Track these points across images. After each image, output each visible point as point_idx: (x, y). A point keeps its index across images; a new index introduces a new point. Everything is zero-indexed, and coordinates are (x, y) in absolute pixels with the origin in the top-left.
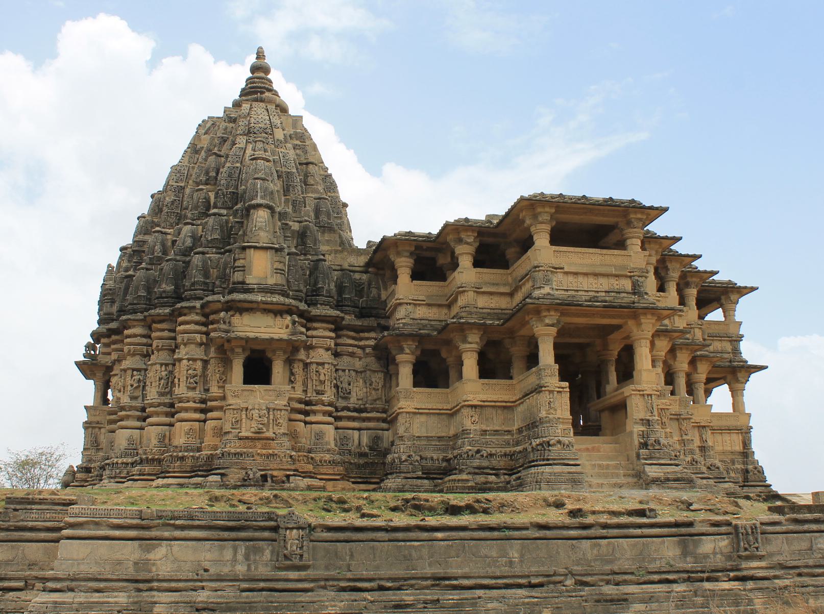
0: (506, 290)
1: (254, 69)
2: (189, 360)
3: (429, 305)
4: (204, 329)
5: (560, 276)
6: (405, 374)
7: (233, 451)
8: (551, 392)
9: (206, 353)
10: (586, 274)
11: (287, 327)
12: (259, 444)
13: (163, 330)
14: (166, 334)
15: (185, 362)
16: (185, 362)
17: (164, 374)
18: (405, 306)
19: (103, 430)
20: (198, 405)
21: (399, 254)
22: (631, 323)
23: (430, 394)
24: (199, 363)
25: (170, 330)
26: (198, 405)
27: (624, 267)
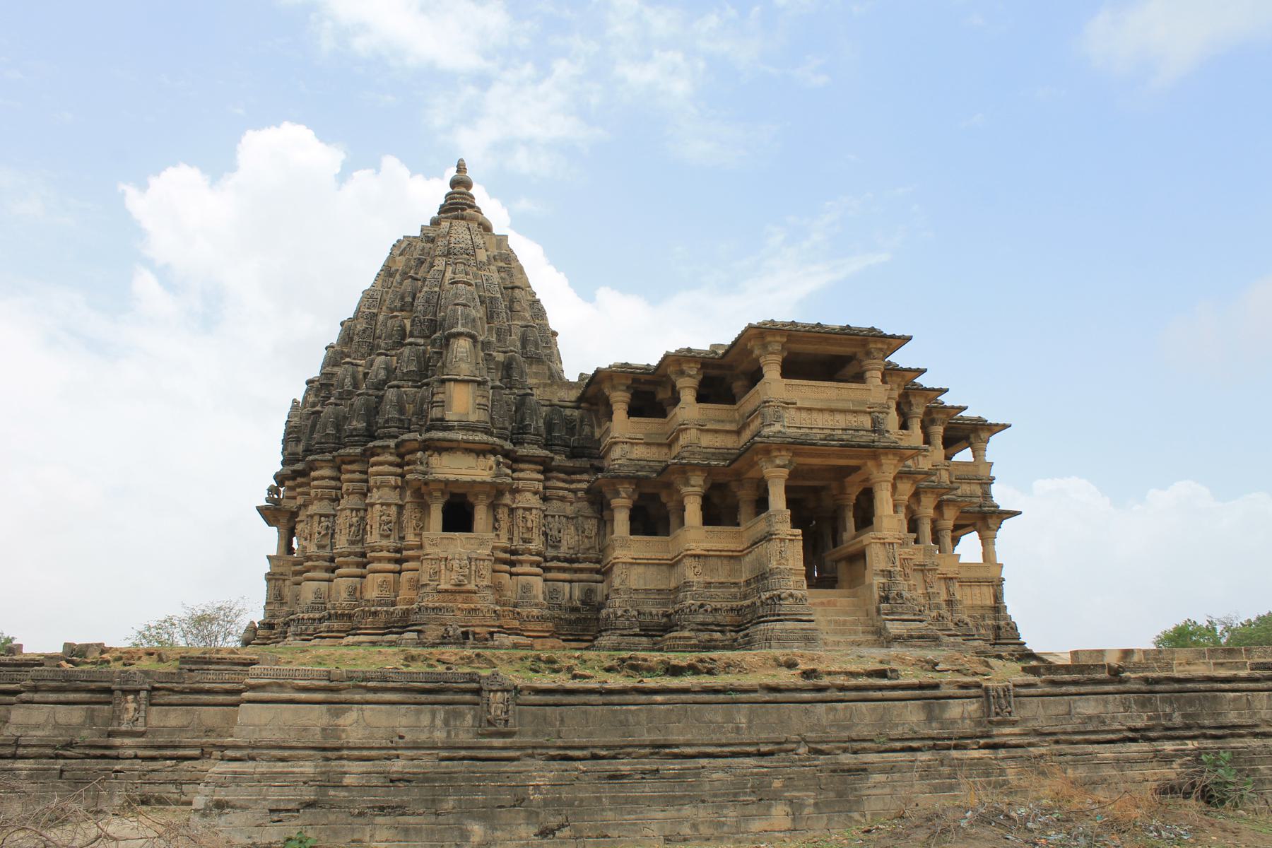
0: (733, 427)
1: (454, 183)
2: (382, 504)
3: (647, 444)
4: (399, 470)
5: (793, 412)
6: (621, 521)
7: (431, 605)
8: (782, 540)
9: (402, 497)
10: (821, 410)
11: (491, 468)
12: (459, 597)
13: (354, 472)
14: (357, 476)
15: (378, 507)
16: (378, 507)
17: (355, 520)
18: (621, 446)
19: (287, 583)
20: (393, 555)
21: (614, 388)
22: (870, 463)
23: (648, 542)
24: (394, 509)
25: (361, 472)
26: (393, 555)
27: (863, 403)
